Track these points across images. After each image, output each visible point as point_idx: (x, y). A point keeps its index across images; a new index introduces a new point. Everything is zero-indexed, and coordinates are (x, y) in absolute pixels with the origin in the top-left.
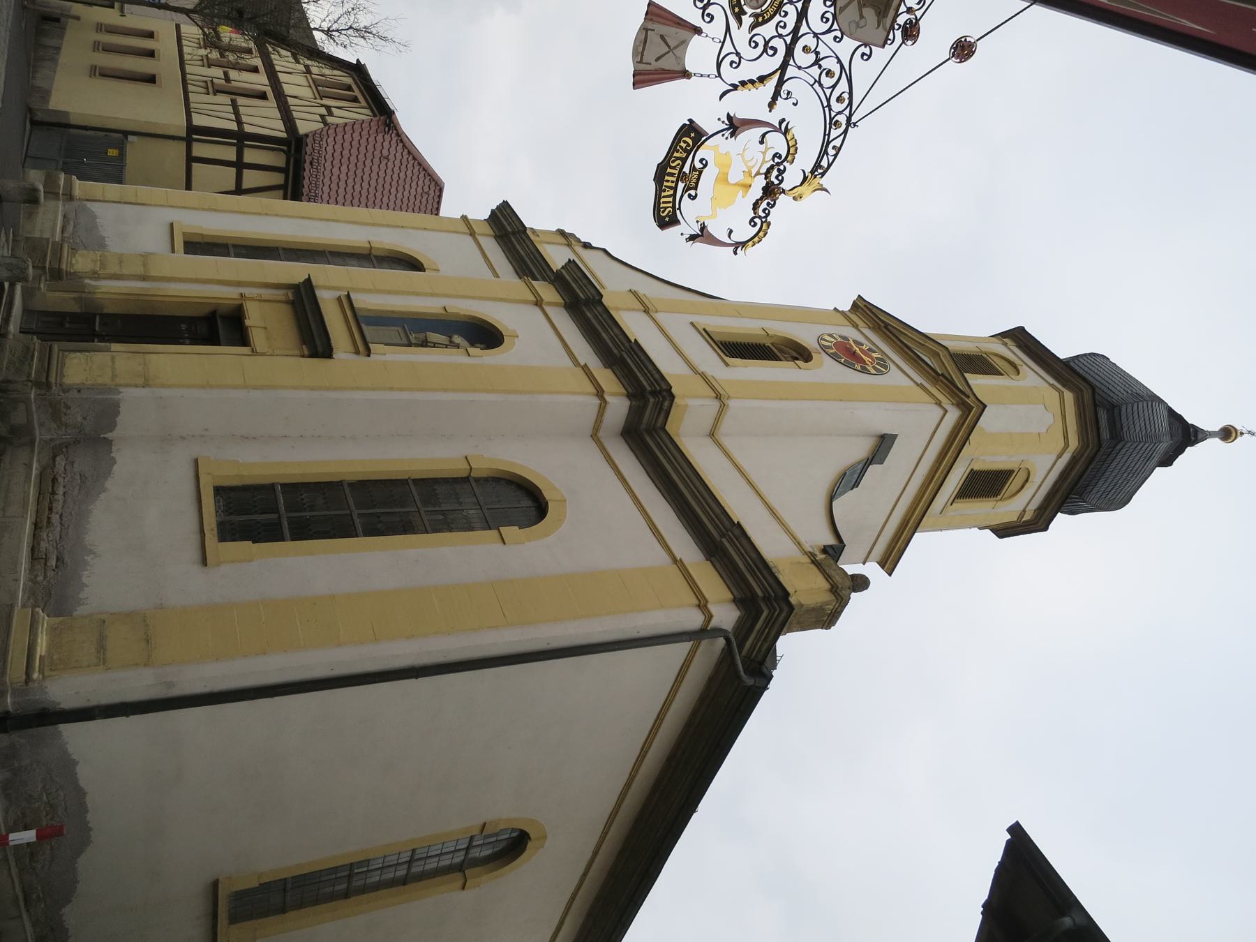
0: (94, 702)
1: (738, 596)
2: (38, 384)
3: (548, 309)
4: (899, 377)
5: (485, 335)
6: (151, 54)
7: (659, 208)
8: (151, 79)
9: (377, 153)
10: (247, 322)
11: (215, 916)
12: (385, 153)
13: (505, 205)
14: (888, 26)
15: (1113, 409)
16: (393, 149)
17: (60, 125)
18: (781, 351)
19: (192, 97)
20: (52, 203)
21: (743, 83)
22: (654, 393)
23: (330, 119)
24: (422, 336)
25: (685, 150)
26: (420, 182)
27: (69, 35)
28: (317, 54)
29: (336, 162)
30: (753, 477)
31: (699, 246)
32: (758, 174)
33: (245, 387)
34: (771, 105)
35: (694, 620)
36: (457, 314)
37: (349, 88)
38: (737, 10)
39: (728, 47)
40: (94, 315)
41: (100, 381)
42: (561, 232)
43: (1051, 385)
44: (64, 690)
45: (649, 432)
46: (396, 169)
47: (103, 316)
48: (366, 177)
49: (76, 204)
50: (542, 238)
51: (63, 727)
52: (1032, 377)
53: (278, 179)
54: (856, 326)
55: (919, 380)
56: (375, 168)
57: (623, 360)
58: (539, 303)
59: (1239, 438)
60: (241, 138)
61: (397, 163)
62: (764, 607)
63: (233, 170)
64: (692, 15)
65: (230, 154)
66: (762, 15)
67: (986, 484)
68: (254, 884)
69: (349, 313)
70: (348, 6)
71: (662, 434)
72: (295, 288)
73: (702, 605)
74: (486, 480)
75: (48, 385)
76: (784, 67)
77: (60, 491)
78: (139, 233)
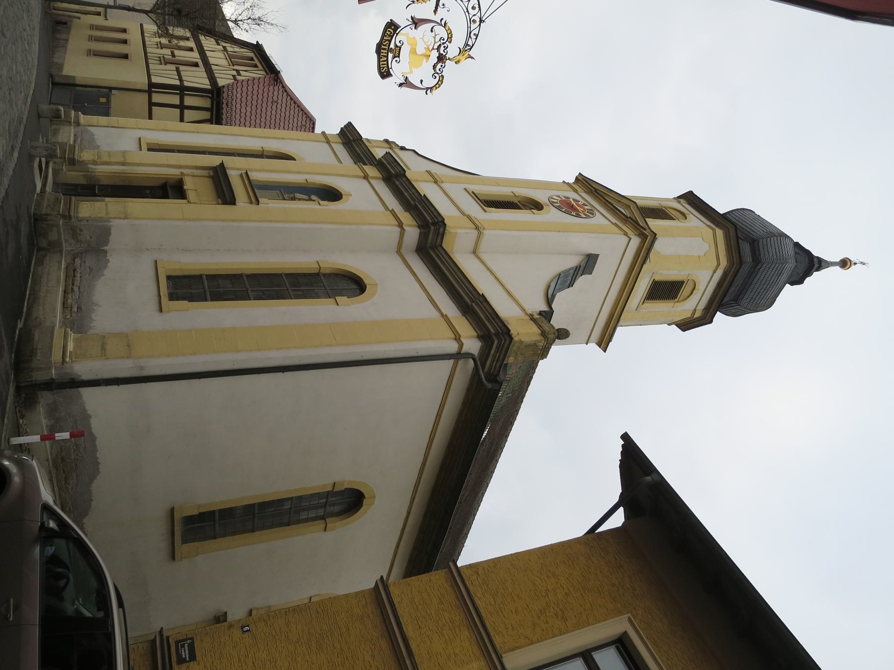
0: (99, 377)
2: (64, 217)
3: (372, 181)
4: (602, 219)
5: (332, 195)
6: (125, 42)
8: (126, 57)
9: (270, 99)
10: (185, 187)
11: (173, 533)
12: (275, 99)
13: (350, 124)
15: (754, 243)
16: (280, 96)
17: (70, 85)
18: (524, 205)
19: (151, 66)
20: (67, 128)
22: (434, 224)
23: (238, 78)
24: (292, 195)
26: (300, 119)
27: (73, 32)
28: (230, 38)
29: (243, 104)
30: (499, 275)
31: (404, 89)
32: (433, 49)
33: (184, 219)
34: (435, 11)
35: (453, 347)
36: (314, 183)
37: (252, 59)
40: (95, 186)
41: (99, 215)
42: (386, 141)
43: (708, 226)
44: (84, 369)
45: (432, 248)
46: (283, 110)
47: (100, 186)
48: (263, 115)
49: (81, 128)
50: (373, 144)
52: (695, 221)
53: (206, 115)
54: (576, 191)
55: (614, 221)
56: (269, 108)
57: (416, 206)
58: (366, 177)
59: (853, 266)
60: (182, 90)
61: (284, 105)
62: (495, 338)
63: (178, 111)
65: (176, 100)
67: (665, 291)
68: (195, 512)
69: (247, 182)
70: (248, 5)
71: (439, 248)
72: (214, 169)
73: (458, 338)
74: (330, 274)
75: (70, 217)
77: (78, 275)
78: (120, 141)
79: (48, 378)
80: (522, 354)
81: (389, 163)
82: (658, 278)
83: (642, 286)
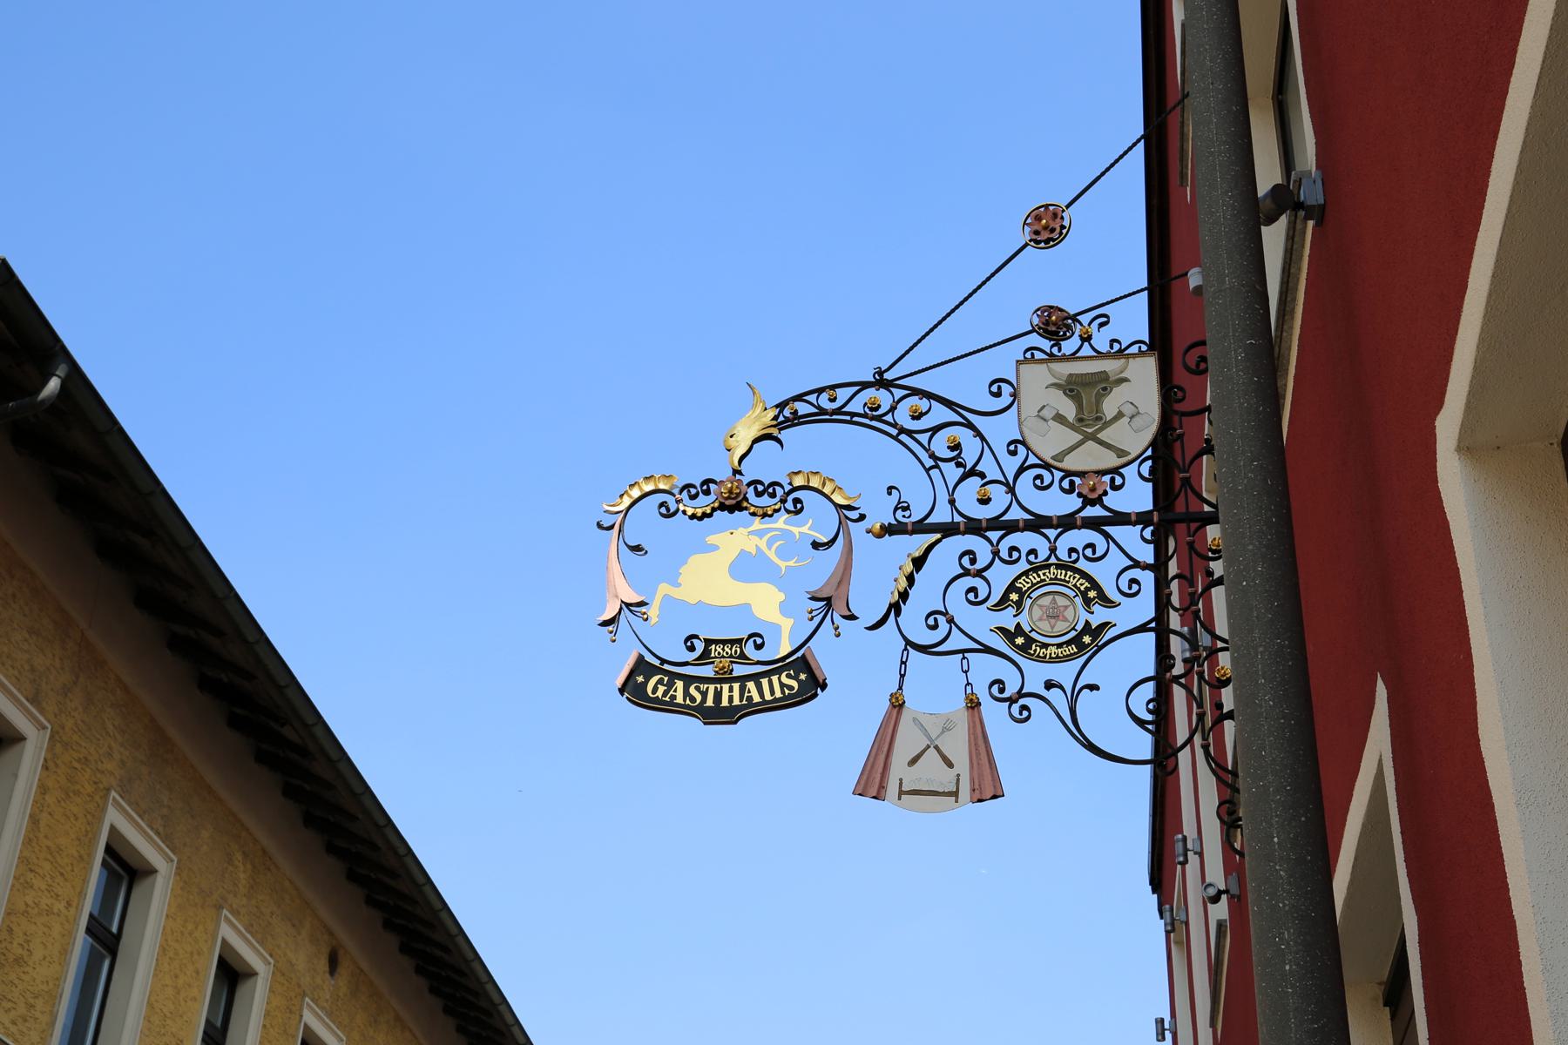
7: (785, 698)
14: (1120, 362)
21: (904, 596)
25: (670, 685)
38: (1087, 639)
66: (1084, 594)
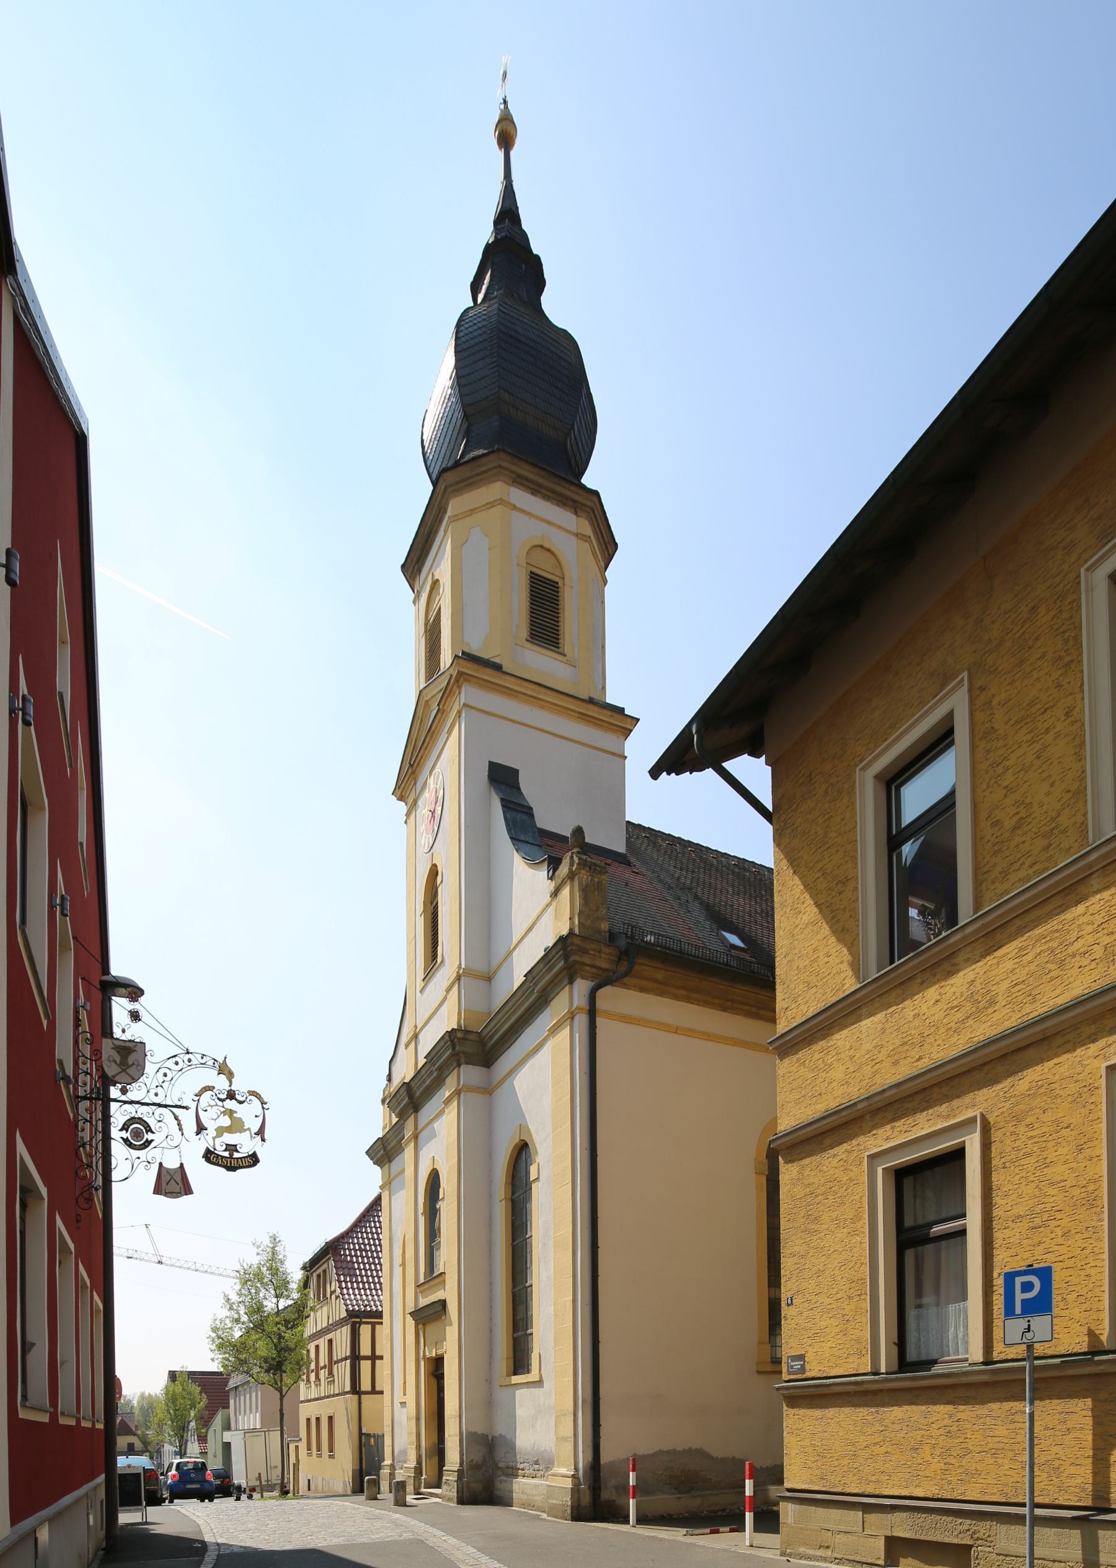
1: (566, 981)
8: (331, 1418)
34: (186, 1108)
39: (164, 1145)
51: (602, 1462)
64: (155, 1168)
76: (166, 1106)
79: (588, 1492)
80: (597, 910)
81: (399, 1104)
82: (524, 633)
83: (537, 662)
